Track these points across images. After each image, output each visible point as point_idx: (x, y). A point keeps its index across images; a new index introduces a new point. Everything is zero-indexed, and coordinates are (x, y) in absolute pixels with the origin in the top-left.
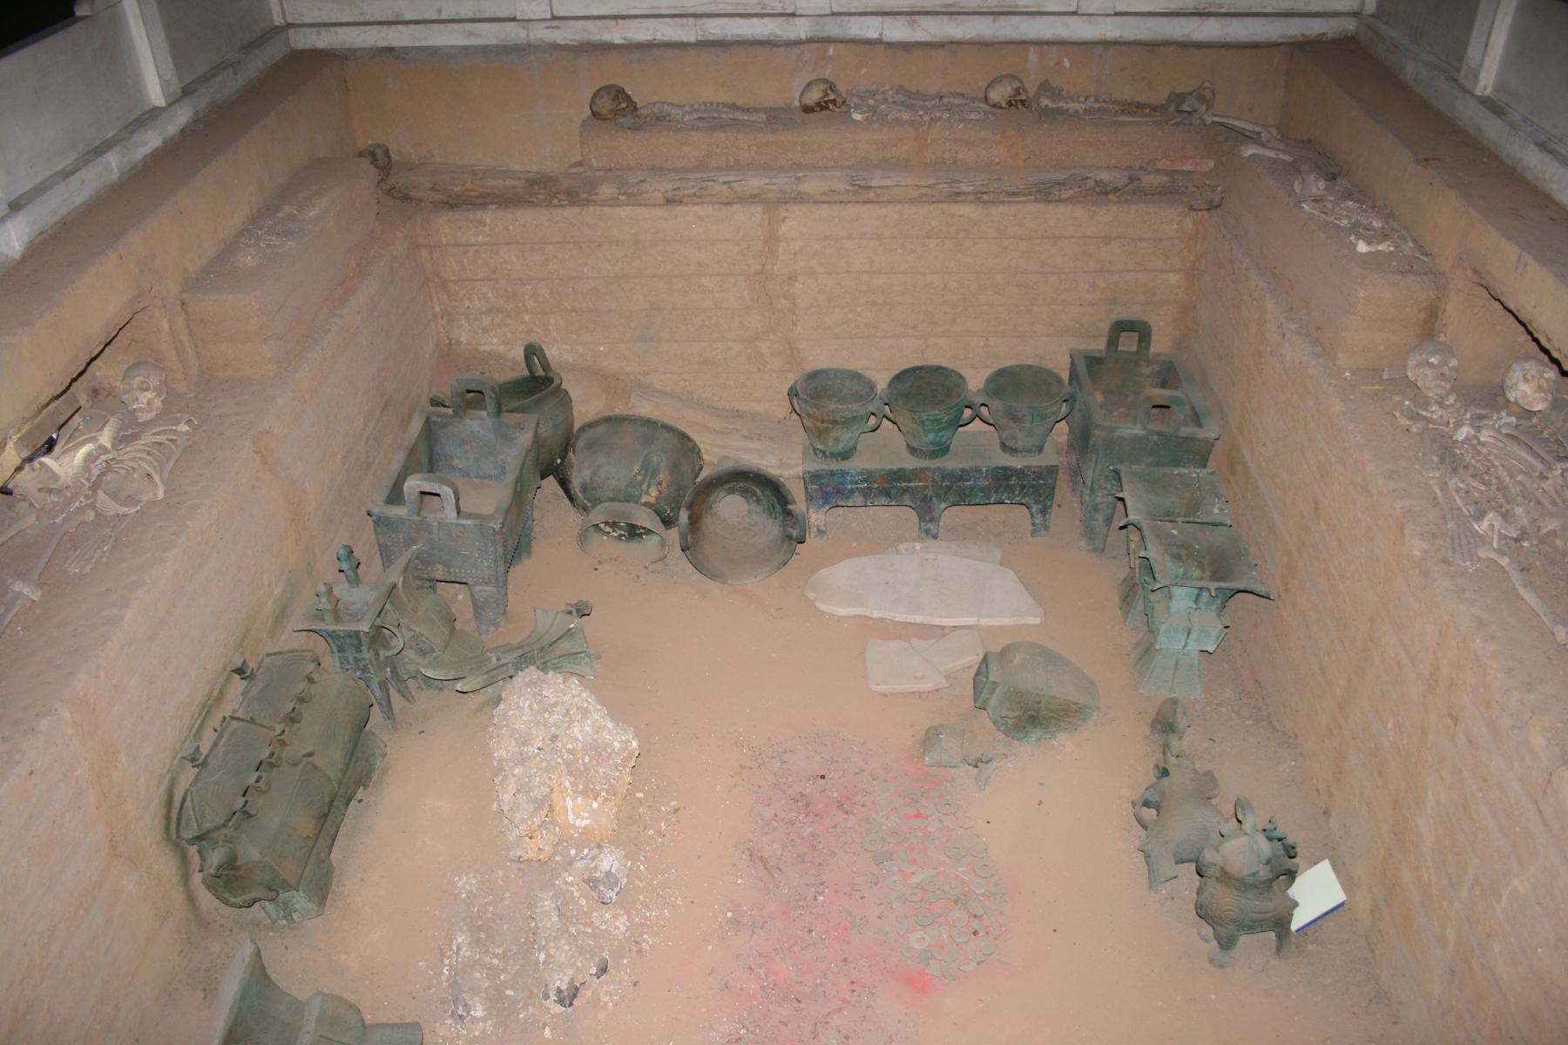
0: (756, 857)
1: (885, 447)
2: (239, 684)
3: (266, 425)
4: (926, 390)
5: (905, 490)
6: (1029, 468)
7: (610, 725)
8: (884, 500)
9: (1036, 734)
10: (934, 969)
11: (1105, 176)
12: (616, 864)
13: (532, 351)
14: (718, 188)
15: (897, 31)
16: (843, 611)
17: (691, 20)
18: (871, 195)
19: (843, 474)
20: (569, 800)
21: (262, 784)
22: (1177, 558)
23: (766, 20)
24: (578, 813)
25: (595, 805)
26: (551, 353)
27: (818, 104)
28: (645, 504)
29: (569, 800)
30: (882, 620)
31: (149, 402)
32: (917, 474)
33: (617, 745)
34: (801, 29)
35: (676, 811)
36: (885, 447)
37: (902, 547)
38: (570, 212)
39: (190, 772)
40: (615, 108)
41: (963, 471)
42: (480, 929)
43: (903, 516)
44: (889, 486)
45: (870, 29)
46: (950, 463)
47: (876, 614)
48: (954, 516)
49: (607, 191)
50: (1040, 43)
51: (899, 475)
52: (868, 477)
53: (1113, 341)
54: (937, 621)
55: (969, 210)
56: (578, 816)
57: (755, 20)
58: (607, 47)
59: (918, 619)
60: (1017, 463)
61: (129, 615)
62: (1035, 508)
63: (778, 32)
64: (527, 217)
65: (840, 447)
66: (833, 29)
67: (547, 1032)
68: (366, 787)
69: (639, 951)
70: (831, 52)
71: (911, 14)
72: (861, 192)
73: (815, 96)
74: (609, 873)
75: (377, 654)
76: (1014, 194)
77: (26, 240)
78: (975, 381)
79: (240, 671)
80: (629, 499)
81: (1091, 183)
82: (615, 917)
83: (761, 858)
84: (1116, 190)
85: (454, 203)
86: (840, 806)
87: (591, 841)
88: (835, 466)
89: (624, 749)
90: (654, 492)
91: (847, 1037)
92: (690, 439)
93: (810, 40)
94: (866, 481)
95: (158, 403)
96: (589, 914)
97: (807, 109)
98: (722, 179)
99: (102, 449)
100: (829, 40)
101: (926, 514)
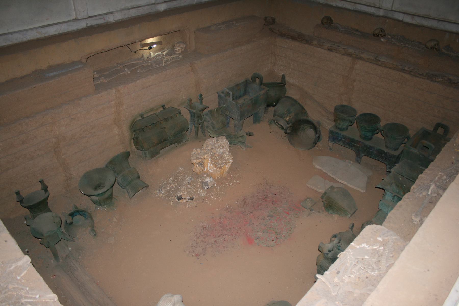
0: (244, 201)
1: (354, 132)
2: (162, 109)
3: (196, 62)
4: (370, 121)
5: (354, 146)
6: (388, 153)
7: (227, 153)
8: (347, 146)
9: (331, 212)
10: (257, 241)
11: (452, 77)
12: (209, 182)
13: (283, 77)
14: (341, 49)
15: (408, 19)
16: (318, 167)
17: (353, 4)
18: (380, 63)
19: (339, 134)
20: (209, 164)
21: (150, 127)
22: (397, 186)
23: (372, 8)
24: (210, 167)
25: (215, 169)
26: (287, 79)
27: (377, 34)
28: (285, 120)
29: (209, 164)
30: (325, 173)
31: (179, 50)
32: (358, 142)
33: (227, 158)
34: (381, 13)
35: (237, 183)
36: (354, 132)
37: (347, 161)
38: (306, 46)
39: (140, 118)
40: (327, 22)
41: (370, 146)
42: (176, 179)
43: (351, 153)
44: (350, 143)
45: (400, 17)
46: (368, 143)
47: (324, 171)
48: (365, 159)
49: (315, 42)
50: (451, 33)
51: (353, 140)
52: (345, 137)
53: (436, 128)
54: (337, 179)
55: (407, 76)
56: (210, 169)
57: (370, 8)
58: (331, 6)
59: (333, 176)
60: (386, 150)
61: (138, 81)
62: (388, 166)
63: (375, 12)
64: (296, 44)
65: (340, 126)
66: (390, 15)
67: (172, 203)
68: (178, 144)
69: (203, 202)
70: (387, 21)
71: (413, 15)
72: (376, 61)
73: (377, 32)
74: (206, 182)
75: (198, 120)
76: (421, 75)
77: (165, 8)
78: (382, 123)
79: (163, 106)
80: (281, 117)
81: (446, 79)
82: (203, 192)
83: (245, 201)
84: (454, 83)
85: (282, 35)
86: (273, 202)
87: (210, 175)
88: (338, 131)
89: (227, 160)
90: (288, 118)
91: (225, 240)
92: (305, 110)
93: (383, 16)
94: (344, 138)
95: (180, 51)
96: (198, 188)
97: (374, 35)
98: (343, 47)
99: (163, 55)
100: (388, 18)
101: (358, 155)
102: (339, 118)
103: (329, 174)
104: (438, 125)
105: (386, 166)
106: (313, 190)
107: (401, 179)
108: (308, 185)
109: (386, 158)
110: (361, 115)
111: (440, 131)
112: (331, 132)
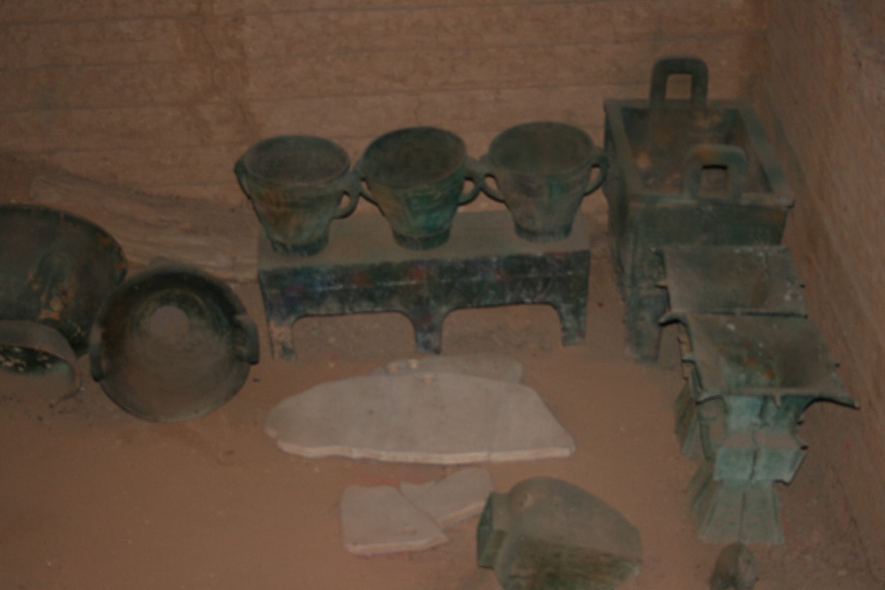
5: (394, 291)
6: (552, 255)
19: (309, 272)
22: (737, 360)
28: (46, 322)
30: (364, 461)
32: (407, 269)
36: (366, 234)
37: (393, 366)
41: (467, 262)
43: (390, 325)
44: (371, 287)
46: (449, 254)
47: (356, 454)
48: (458, 322)
51: (383, 272)
52: (344, 275)
53: (658, 88)
54: (435, 459)
59: (411, 457)
60: (536, 249)
62: (564, 307)
65: (305, 237)
78: (477, 146)
88: (300, 262)
92: (104, 234)
94: (340, 280)
101: (424, 322)
102: (294, 205)
103: (385, 456)
104: (666, 68)
105: (556, 307)
106: (400, 554)
107: (732, 327)
108: (360, 548)
109: (546, 281)
110: (368, 153)
111: (678, 89)
112: (270, 280)
